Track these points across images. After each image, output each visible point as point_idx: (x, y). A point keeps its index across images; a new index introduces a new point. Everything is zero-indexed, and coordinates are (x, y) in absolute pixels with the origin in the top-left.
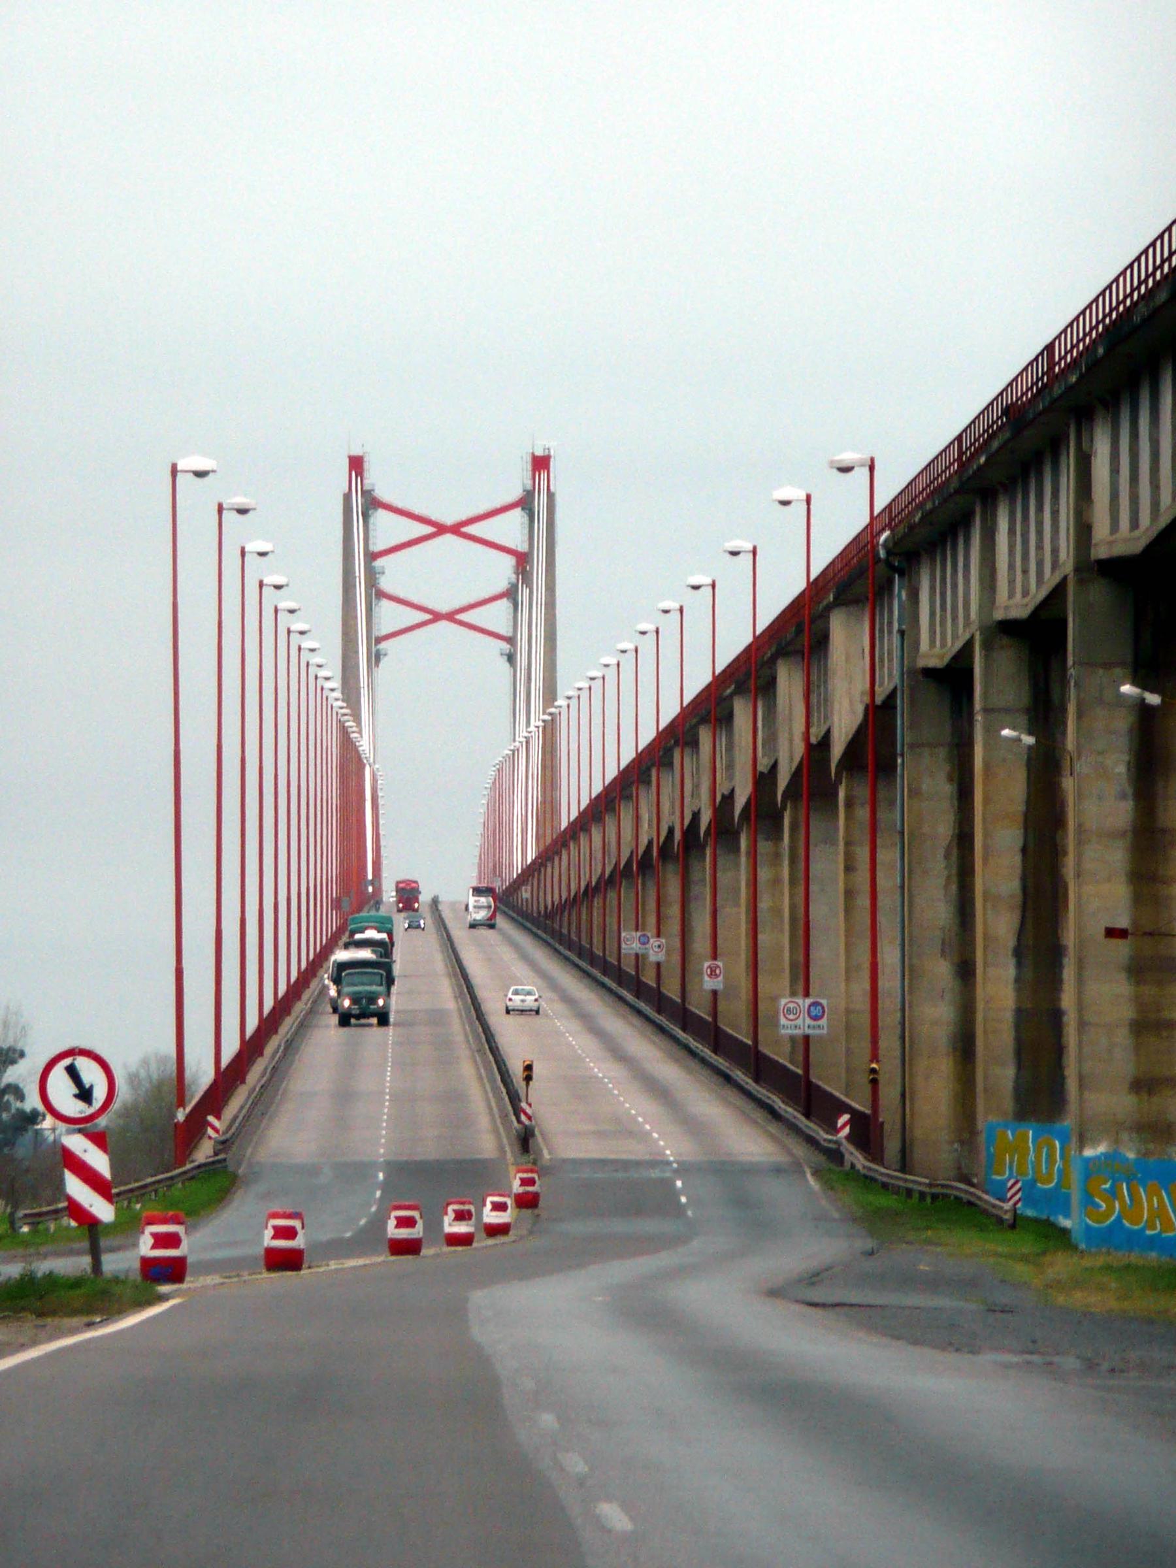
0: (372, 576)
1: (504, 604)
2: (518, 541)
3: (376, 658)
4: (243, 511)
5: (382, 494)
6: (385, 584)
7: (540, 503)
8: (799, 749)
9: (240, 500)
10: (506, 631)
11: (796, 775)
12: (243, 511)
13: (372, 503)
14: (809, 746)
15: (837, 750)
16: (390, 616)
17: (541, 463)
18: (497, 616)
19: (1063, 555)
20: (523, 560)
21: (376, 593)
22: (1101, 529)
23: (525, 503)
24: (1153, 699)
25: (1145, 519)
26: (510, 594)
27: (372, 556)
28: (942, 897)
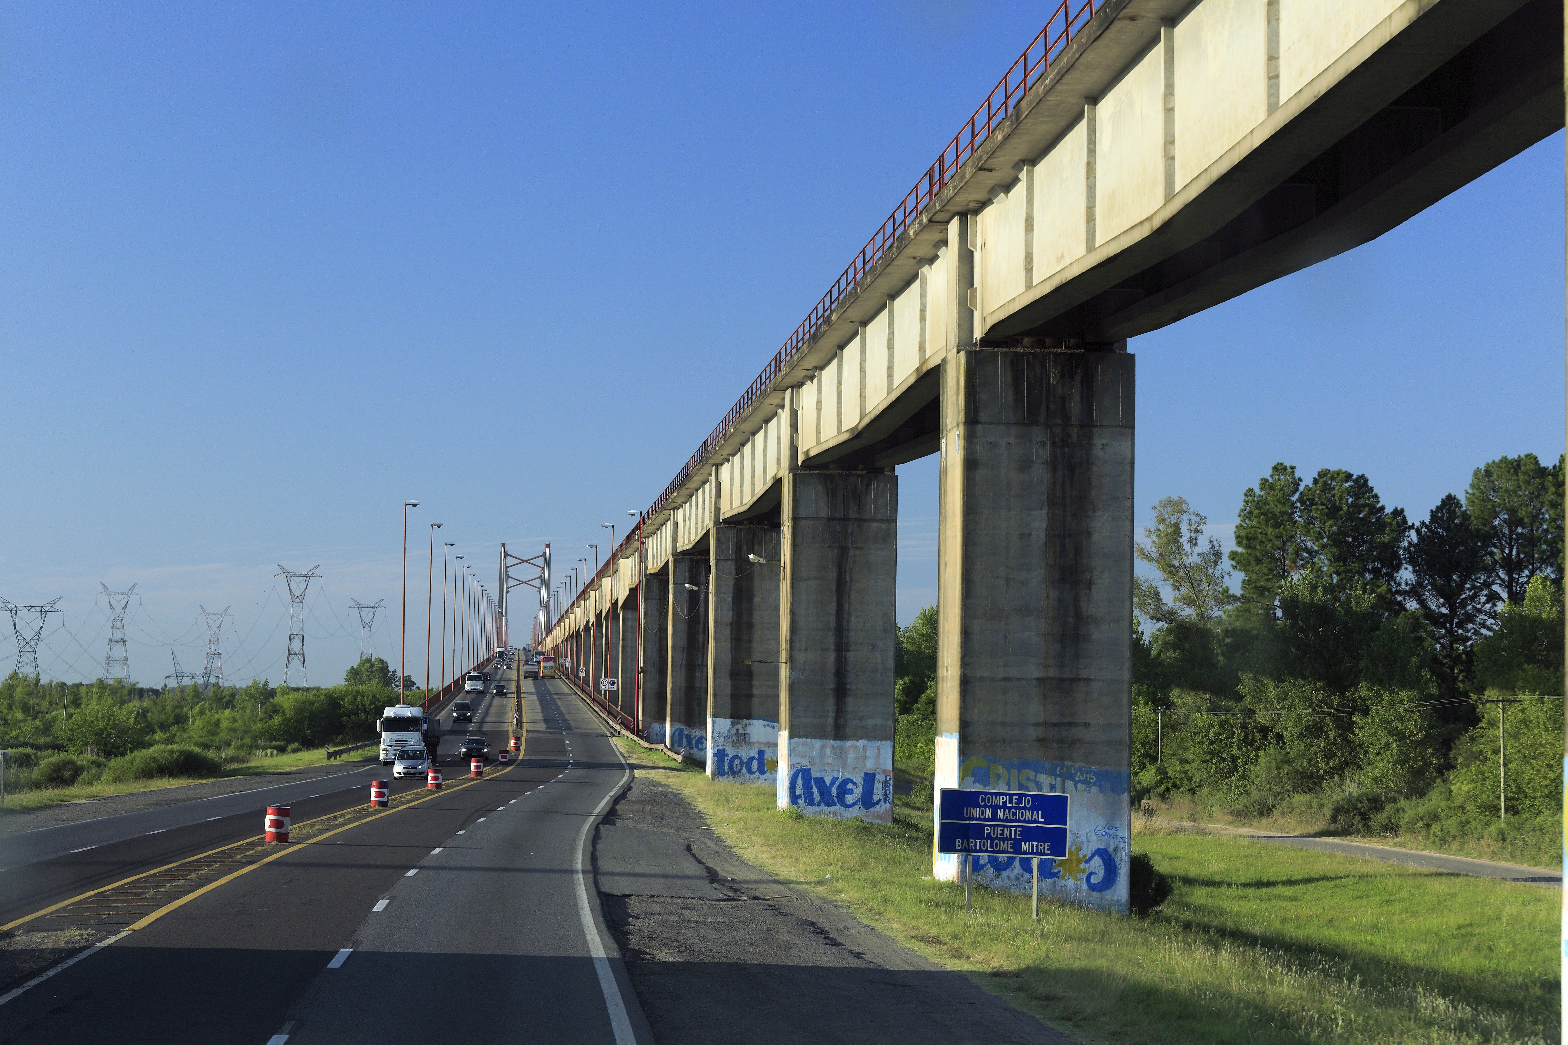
0: (506, 572)
1: (539, 580)
2: (542, 565)
3: (508, 592)
4: (415, 506)
5: (509, 553)
6: (510, 574)
7: (547, 556)
8: (609, 605)
9: (414, 501)
10: (542, 565)
11: (608, 612)
12: (415, 506)
13: (507, 555)
14: (612, 604)
15: (620, 604)
16: (511, 582)
17: (548, 546)
18: (537, 583)
19: (668, 553)
20: (543, 569)
21: (508, 577)
22: (680, 544)
23: (543, 555)
24: (695, 588)
25: (699, 530)
26: (540, 577)
27: (506, 567)
28: (364, 658)
